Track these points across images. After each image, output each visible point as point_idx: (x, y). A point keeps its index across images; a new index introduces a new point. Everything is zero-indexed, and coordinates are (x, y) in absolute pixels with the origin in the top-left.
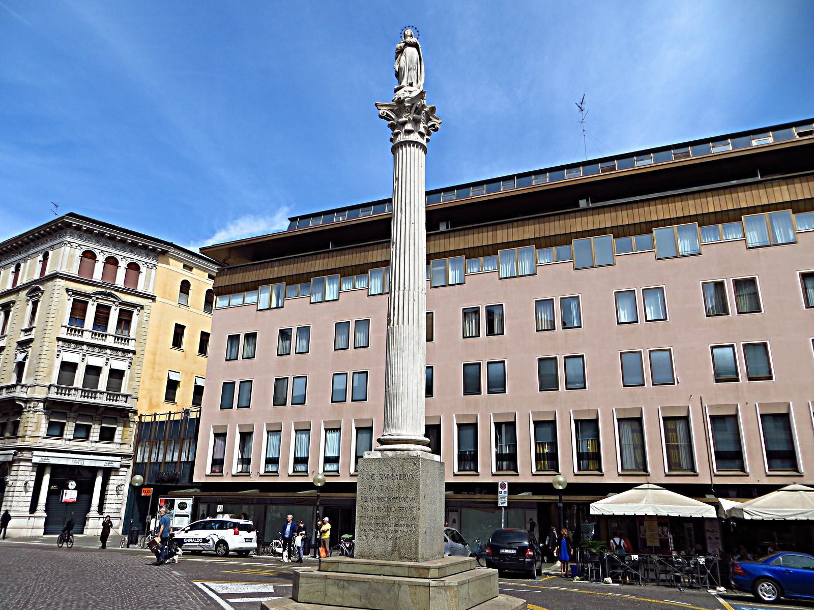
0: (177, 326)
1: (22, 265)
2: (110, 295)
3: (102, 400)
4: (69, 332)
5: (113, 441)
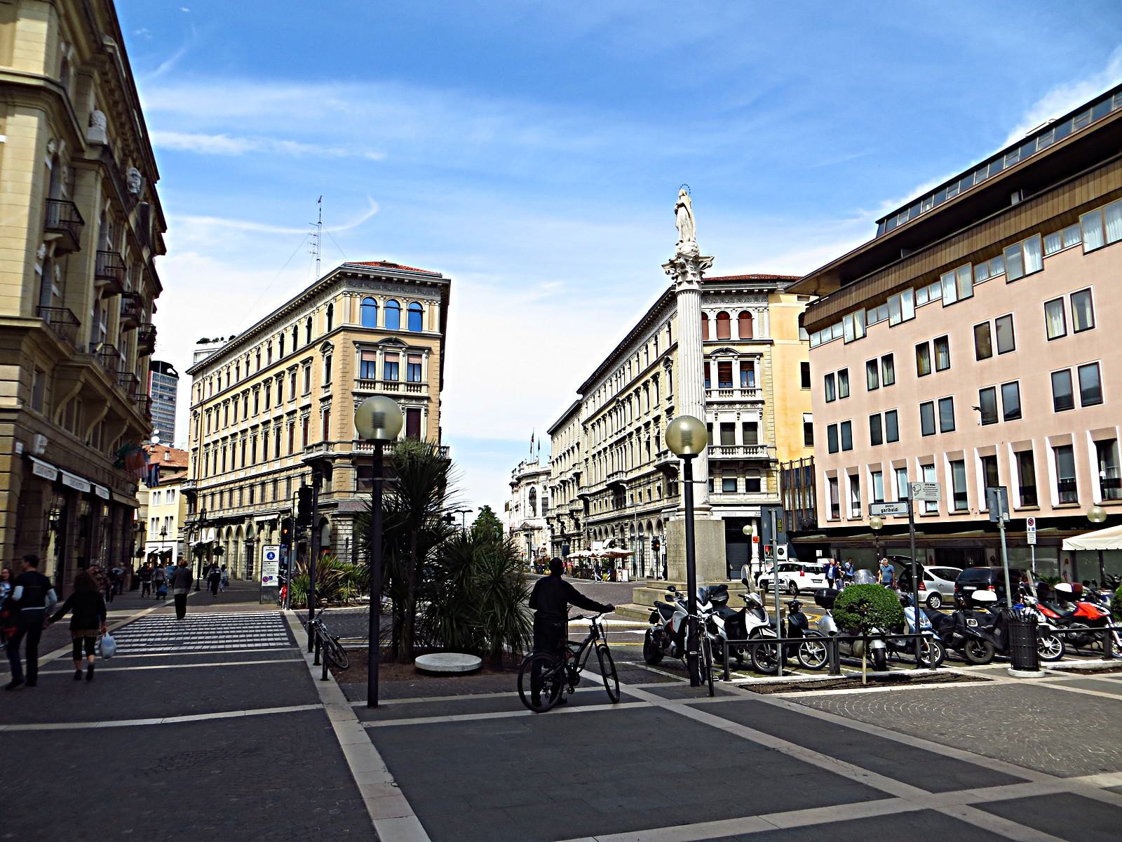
0: (803, 364)
1: (658, 336)
2: (728, 350)
3: (740, 454)
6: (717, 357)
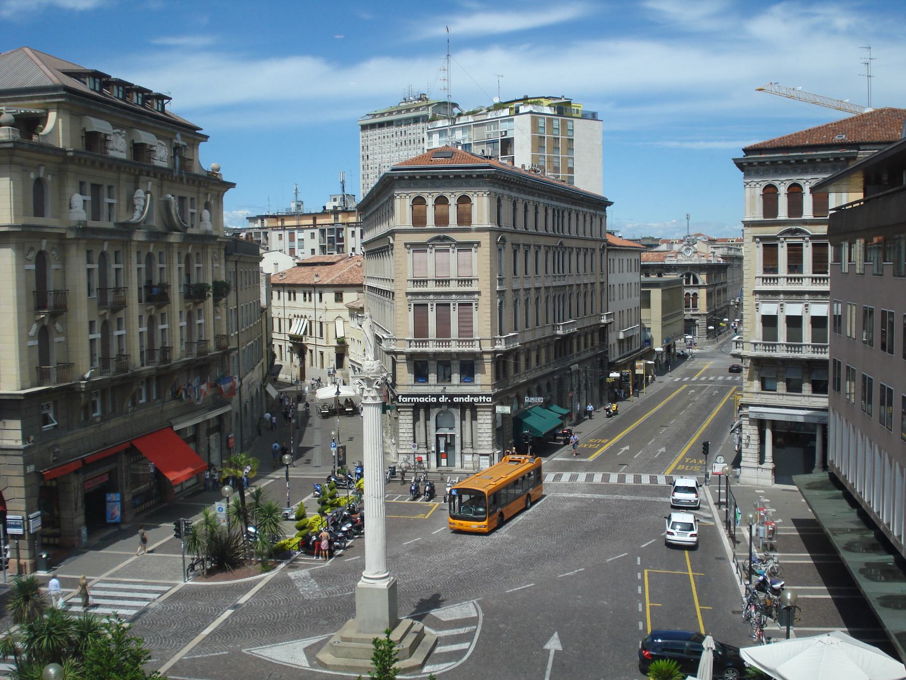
3: (781, 353)
6: (785, 238)
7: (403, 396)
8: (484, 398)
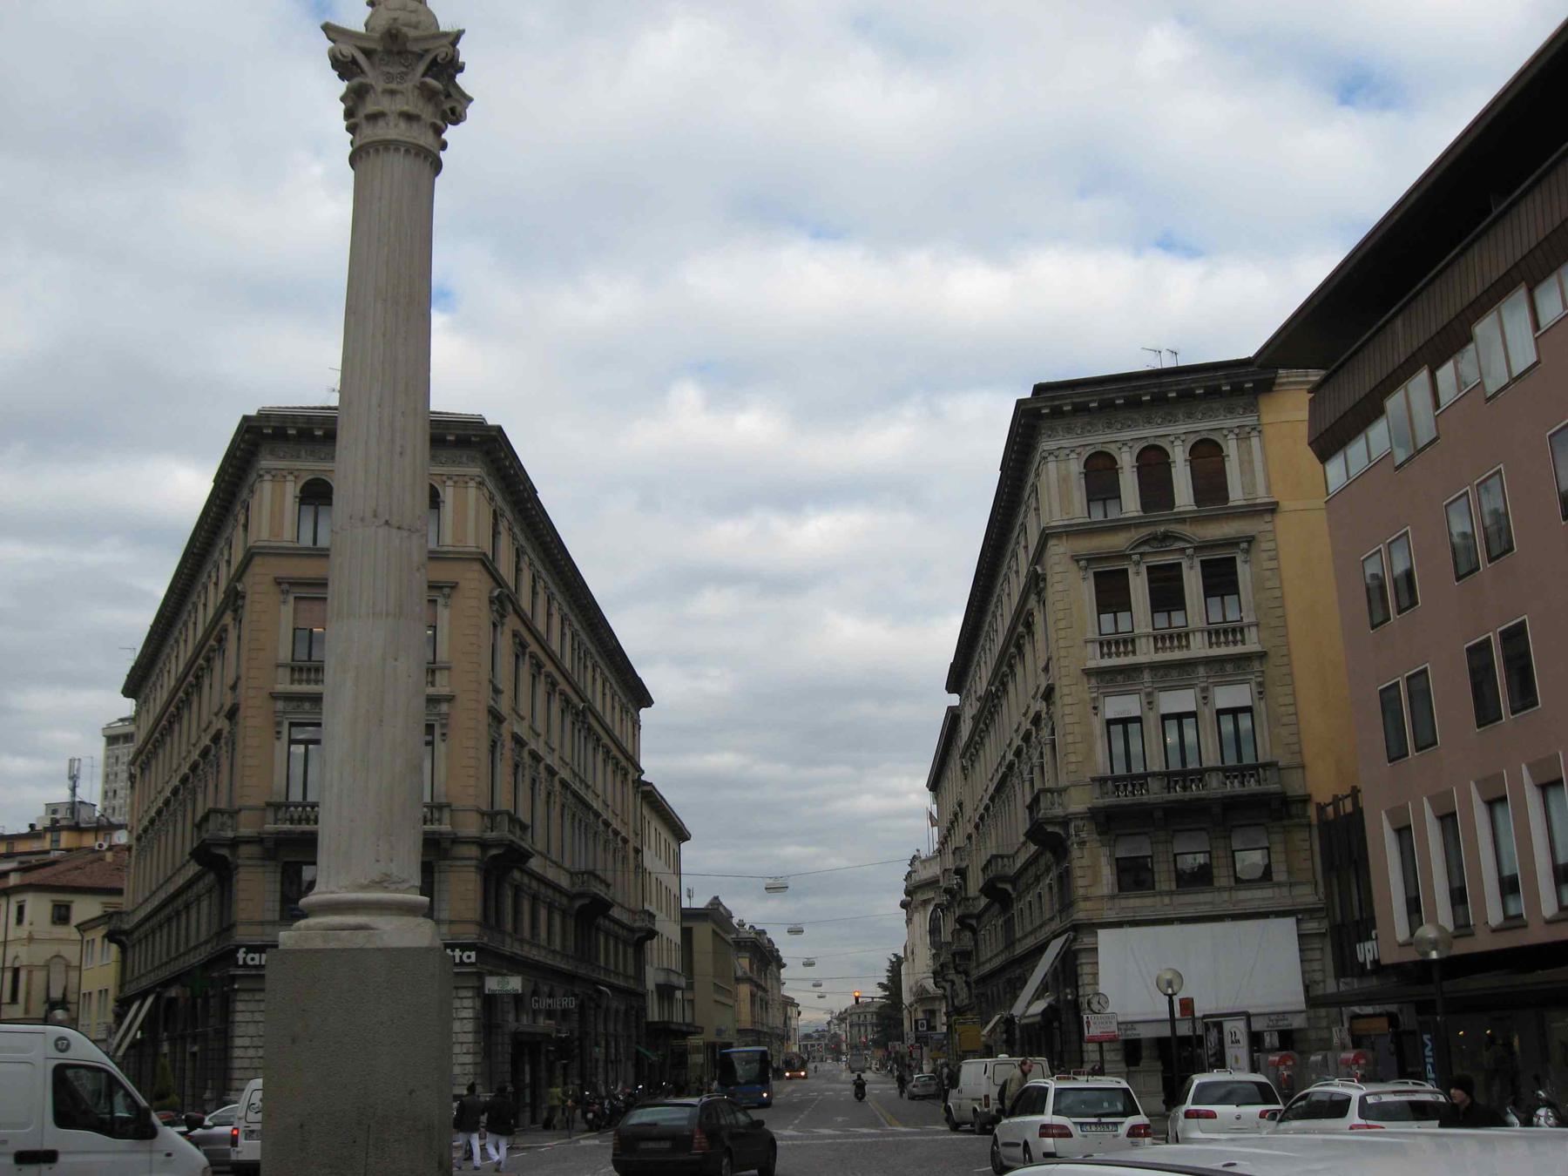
2: (1167, 537)
4: (1160, 645)
5: (1212, 884)
7: (251, 949)
8: (458, 953)
